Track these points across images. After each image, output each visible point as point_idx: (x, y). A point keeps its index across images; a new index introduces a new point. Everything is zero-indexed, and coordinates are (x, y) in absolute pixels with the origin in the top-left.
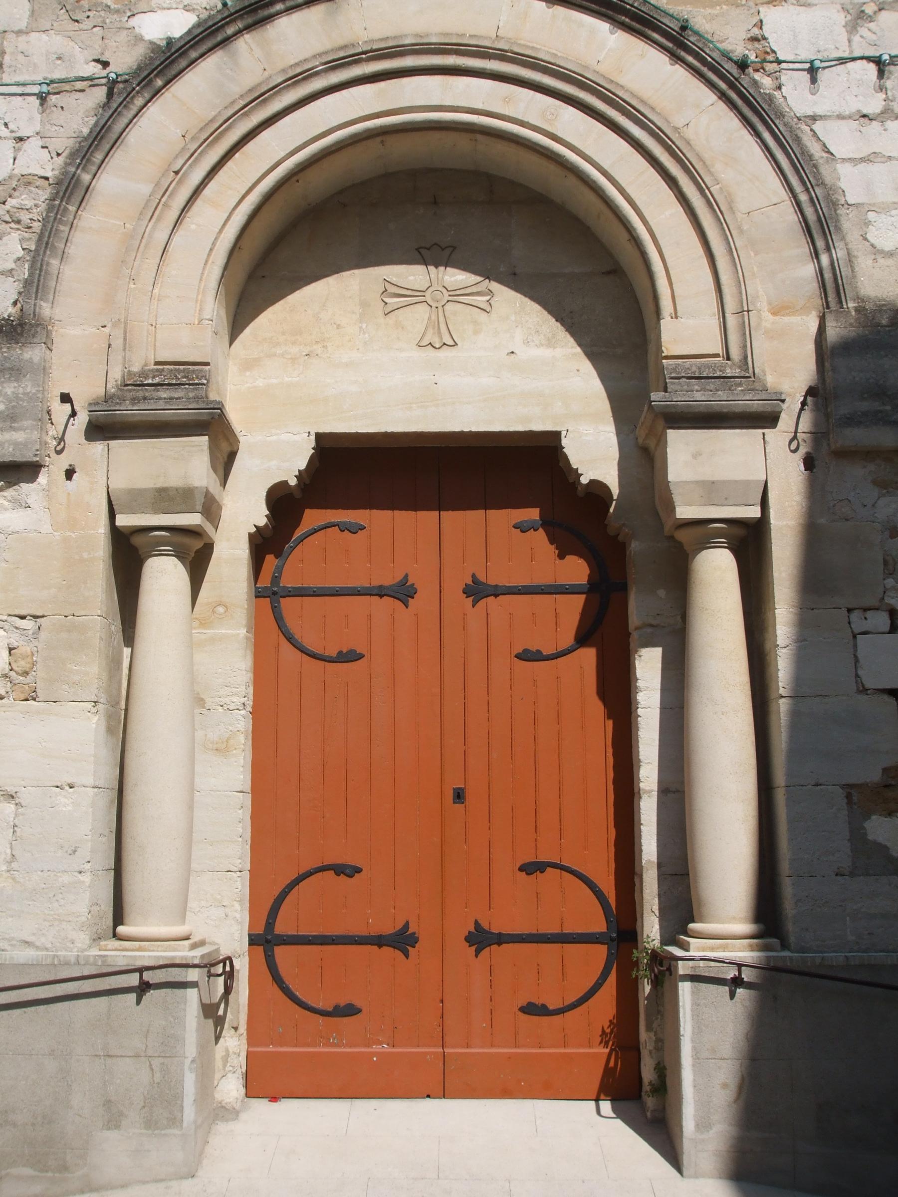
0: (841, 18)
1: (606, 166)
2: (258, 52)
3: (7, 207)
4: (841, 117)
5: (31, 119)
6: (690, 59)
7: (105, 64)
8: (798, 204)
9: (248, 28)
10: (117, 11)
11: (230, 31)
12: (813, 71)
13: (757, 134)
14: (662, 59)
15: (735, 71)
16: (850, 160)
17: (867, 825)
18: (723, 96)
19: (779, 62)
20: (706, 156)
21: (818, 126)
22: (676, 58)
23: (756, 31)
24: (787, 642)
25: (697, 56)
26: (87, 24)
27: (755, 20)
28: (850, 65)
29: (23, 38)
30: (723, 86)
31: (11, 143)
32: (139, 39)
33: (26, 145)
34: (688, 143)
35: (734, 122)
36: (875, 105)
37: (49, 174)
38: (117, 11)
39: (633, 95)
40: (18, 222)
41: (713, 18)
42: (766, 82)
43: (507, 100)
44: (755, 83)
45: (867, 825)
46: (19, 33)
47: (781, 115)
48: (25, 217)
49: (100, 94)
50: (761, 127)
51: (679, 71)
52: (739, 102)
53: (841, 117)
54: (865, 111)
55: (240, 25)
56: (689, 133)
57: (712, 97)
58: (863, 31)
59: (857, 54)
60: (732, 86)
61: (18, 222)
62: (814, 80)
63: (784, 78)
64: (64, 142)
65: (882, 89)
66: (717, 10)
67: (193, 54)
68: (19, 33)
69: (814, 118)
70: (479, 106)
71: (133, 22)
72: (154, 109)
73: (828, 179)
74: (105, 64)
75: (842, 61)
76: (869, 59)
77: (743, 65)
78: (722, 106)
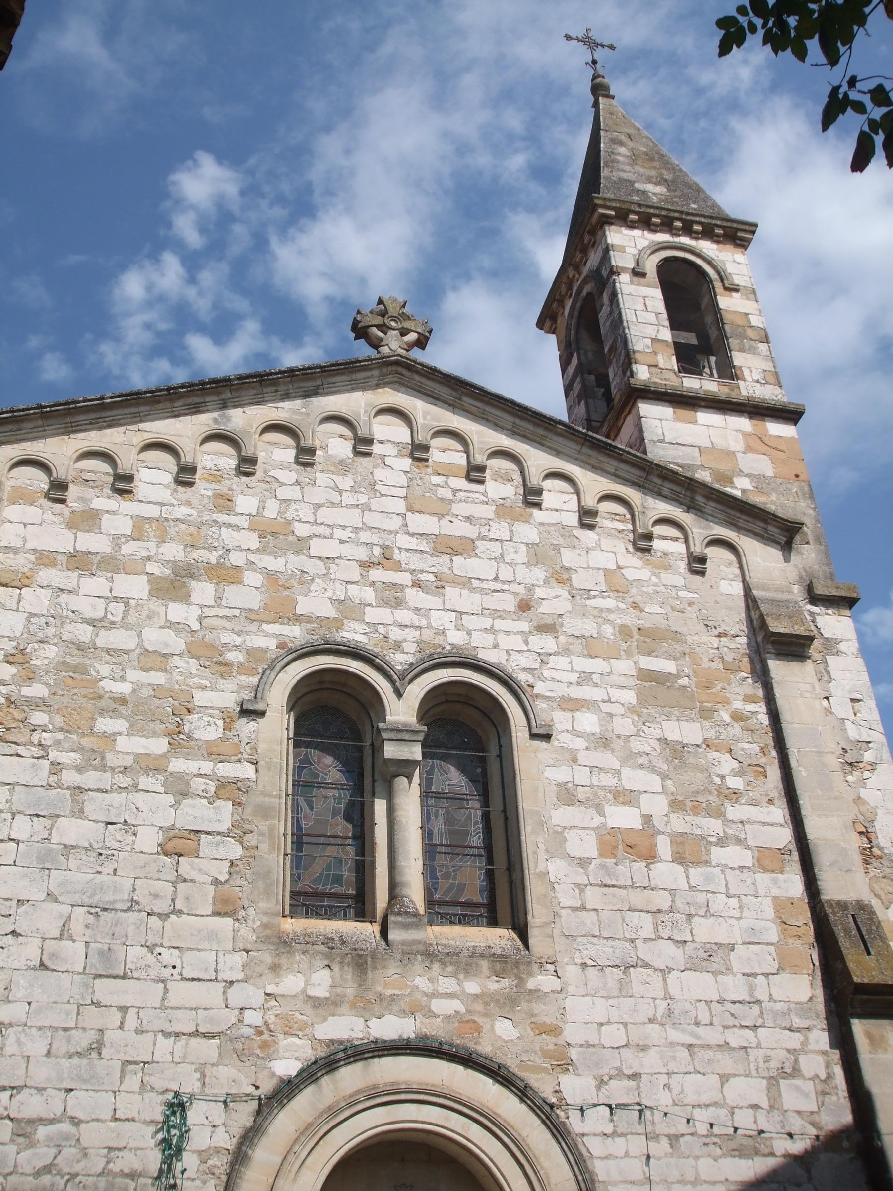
0: (593, 1083)
1: (491, 1156)
2: (331, 1086)
3: (208, 1165)
4: (595, 1135)
5: (220, 1115)
6: (529, 1102)
7: (257, 1088)
8: (578, 1180)
9: (327, 1073)
10: (263, 1058)
11: (319, 1075)
12: (582, 1110)
13: (559, 1143)
14: (516, 1100)
15: (549, 1110)
16: (600, 1158)
17: (48, 356)
18: (543, 1121)
19: (567, 1105)
20: (537, 1153)
21: (585, 1139)
22: (522, 1100)
23: (557, 1088)
24: (730, 254)
25: (532, 1101)
26: (247, 1064)
27: (557, 1082)
28: (598, 1107)
29: (215, 1068)
30: (544, 1117)
31: (210, 1128)
32: (273, 1074)
33: (217, 1129)
34: (528, 1146)
35: (549, 1136)
36: (609, 1129)
37: (229, 1148)
38: (263, 1058)
39: (505, 1120)
40: (214, 1174)
41: (538, 1080)
42: (562, 1114)
43: (447, 1119)
44: (558, 1116)
45: (48, 356)
46: (213, 1065)
47: (569, 1133)
48: (217, 1171)
49: (255, 1104)
50: (561, 1140)
51: (523, 1106)
52: (551, 1126)
53: (595, 1135)
54: (605, 1132)
55: (324, 1072)
56: (529, 1141)
57: (538, 1122)
58: (603, 1090)
59: (601, 1102)
60: (548, 1117)
61: (214, 1174)
62: (583, 1115)
63: (570, 1113)
64: (237, 1131)
65: (612, 1120)
66: (540, 1076)
67: (302, 1087)
68: (213, 1065)
69: (583, 1135)
70: (434, 1122)
71: (271, 1064)
72: (281, 1115)
73: (590, 1167)
74: (257, 1088)
75: (595, 1105)
76: (606, 1105)
77: (552, 1106)
78: (543, 1127)
